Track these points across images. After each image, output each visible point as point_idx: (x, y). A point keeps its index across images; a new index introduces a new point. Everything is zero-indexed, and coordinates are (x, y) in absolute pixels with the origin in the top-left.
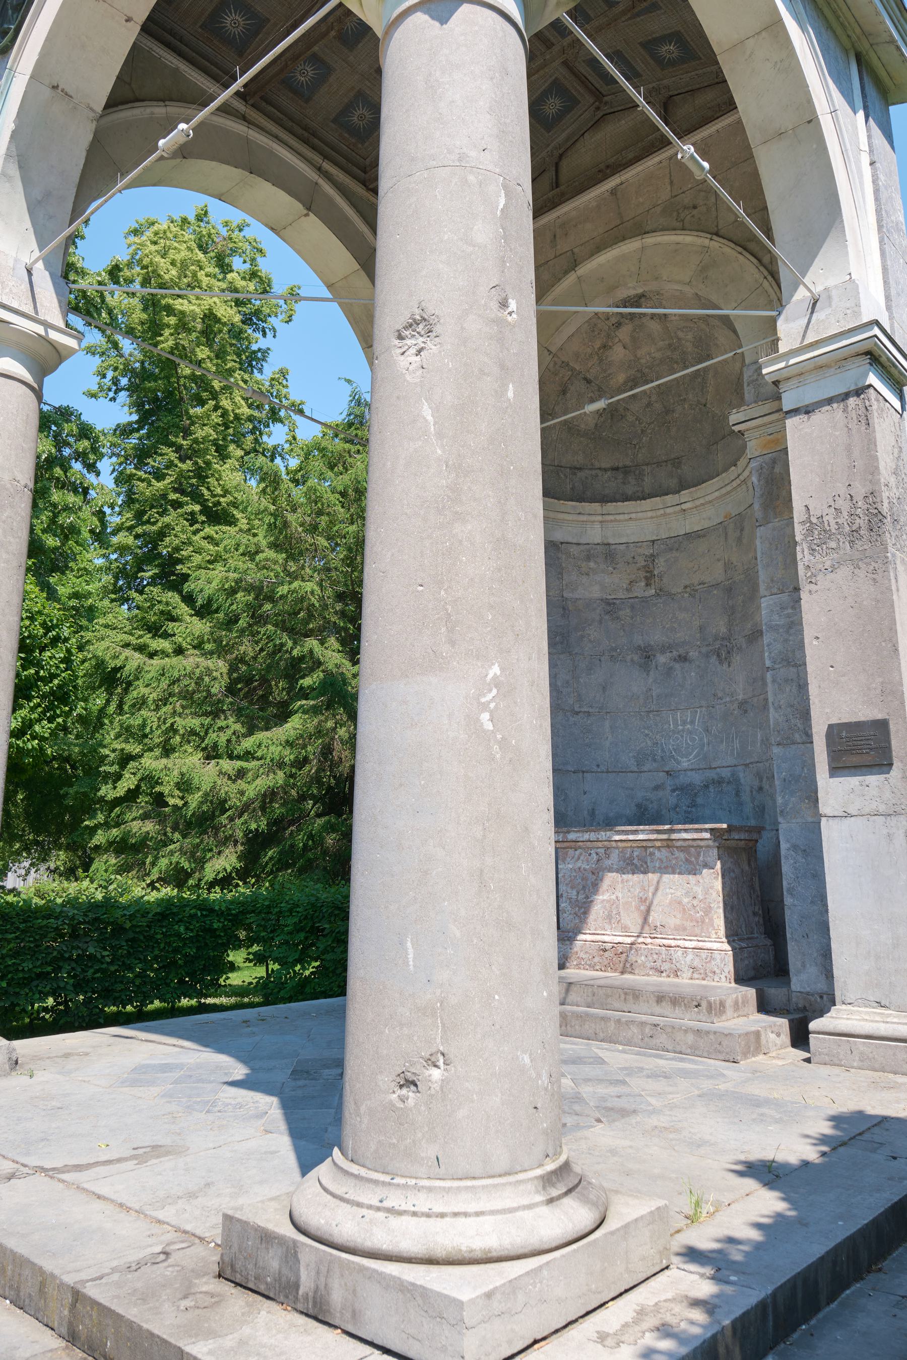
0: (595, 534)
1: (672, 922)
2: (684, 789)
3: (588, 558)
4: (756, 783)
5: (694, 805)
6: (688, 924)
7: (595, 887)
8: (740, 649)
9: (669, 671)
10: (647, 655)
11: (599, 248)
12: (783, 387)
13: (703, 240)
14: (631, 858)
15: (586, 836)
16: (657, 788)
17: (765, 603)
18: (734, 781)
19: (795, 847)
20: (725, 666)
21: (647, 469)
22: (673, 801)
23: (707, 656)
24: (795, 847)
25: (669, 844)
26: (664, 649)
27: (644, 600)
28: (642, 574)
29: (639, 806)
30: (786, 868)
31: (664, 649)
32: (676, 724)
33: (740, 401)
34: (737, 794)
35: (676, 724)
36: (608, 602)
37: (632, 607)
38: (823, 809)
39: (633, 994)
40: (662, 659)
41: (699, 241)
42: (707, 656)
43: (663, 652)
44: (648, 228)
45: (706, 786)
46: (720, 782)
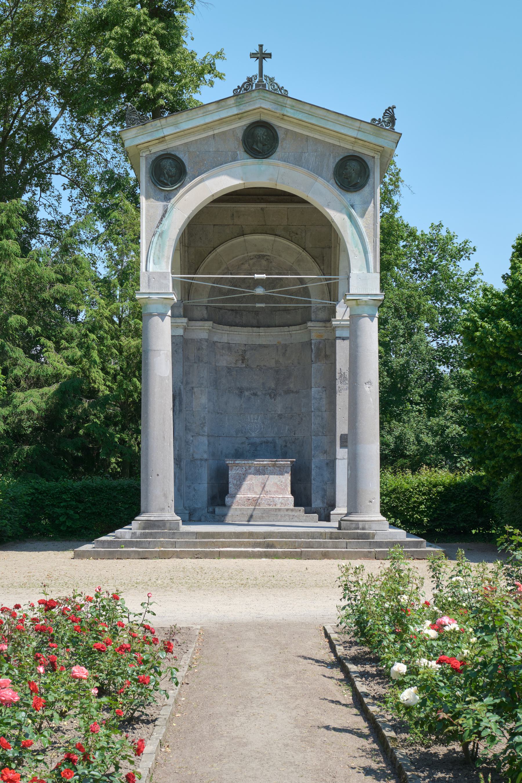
0: (225, 339)
1: (273, 490)
2: (253, 444)
3: (223, 349)
4: (284, 444)
5: (256, 450)
6: (279, 490)
7: (244, 479)
8: (280, 395)
9: (249, 399)
10: (241, 391)
11: (254, 232)
12: (337, 329)
13: (300, 250)
14: (259, 469)
15: (243, 462)
16: (243, 443)
17: (313, 389)
18: (274, 443)
19: (316, 467)
20: (273, 400)
21: (244, 313)
22: (248, 448)
23: (265, 395)
24: (316, 467)
25: (274, 465)
26: (248, 389)
27: (241, 368)
28: (241, 358)
29: (236, 450)
30: (313, 473)
31: (248, 389)
32: (251, 419)
33: (58, 94)
34: (275, 447)
35: (251, 419)
36: (229, 368)
37: (237, 371)
38: (337, 457)
39: (279, 510)
40: (247, 393)
41: (298, 249)
42: (265, 395)
43: (247, 391)
44: (277, 233)
45: (262, 444)
46: (267, 442)
